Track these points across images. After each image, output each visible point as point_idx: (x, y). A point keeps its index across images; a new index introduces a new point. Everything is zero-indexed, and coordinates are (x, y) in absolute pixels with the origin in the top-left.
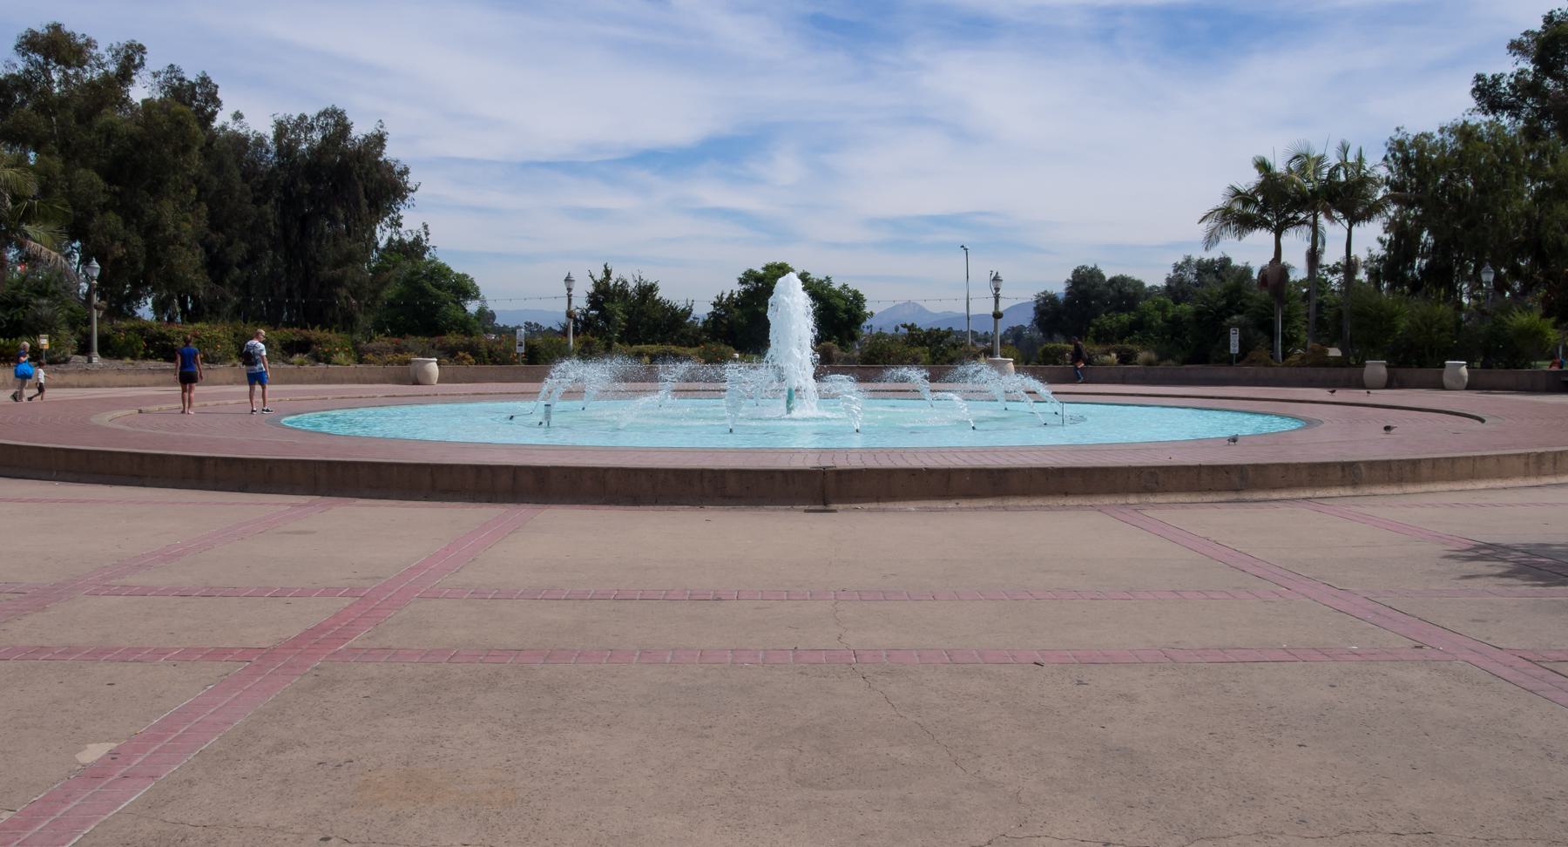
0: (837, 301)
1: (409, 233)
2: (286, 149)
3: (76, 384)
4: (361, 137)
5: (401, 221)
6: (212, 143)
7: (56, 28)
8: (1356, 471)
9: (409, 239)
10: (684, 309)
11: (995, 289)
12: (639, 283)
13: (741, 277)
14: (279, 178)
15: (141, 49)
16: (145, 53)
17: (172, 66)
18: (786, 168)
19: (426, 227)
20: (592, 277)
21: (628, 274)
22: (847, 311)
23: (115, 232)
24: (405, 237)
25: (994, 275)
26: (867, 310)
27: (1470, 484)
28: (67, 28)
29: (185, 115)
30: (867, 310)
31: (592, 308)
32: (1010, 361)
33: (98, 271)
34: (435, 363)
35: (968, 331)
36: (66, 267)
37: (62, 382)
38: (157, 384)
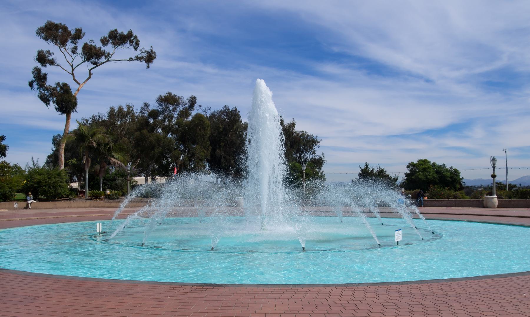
0: (446, 174)
1: (317, 156)
3: (115, 206)
4: (287, 124)
5: (316, 152)
6: (238, 129)
9: (317, 158)
10: (394, 178)
11: (493, 164)
12: (379, 170)
13: (408, 165)
15: (195, 98)
16: (196, 99)
17: (225, 106)
18: (478, 132)
19: (323, 154)
20: (360, 167)
22: (451, 177)
23: (178, 156)
25: (492, 158)
26: (461, 177)
29: (202, 118)
30: (461, 177)
32: (495, 198)
34: (496, 198)
35: (506, 185)
36: (123, 169)
37: (110, 206)
38: (90, 207)
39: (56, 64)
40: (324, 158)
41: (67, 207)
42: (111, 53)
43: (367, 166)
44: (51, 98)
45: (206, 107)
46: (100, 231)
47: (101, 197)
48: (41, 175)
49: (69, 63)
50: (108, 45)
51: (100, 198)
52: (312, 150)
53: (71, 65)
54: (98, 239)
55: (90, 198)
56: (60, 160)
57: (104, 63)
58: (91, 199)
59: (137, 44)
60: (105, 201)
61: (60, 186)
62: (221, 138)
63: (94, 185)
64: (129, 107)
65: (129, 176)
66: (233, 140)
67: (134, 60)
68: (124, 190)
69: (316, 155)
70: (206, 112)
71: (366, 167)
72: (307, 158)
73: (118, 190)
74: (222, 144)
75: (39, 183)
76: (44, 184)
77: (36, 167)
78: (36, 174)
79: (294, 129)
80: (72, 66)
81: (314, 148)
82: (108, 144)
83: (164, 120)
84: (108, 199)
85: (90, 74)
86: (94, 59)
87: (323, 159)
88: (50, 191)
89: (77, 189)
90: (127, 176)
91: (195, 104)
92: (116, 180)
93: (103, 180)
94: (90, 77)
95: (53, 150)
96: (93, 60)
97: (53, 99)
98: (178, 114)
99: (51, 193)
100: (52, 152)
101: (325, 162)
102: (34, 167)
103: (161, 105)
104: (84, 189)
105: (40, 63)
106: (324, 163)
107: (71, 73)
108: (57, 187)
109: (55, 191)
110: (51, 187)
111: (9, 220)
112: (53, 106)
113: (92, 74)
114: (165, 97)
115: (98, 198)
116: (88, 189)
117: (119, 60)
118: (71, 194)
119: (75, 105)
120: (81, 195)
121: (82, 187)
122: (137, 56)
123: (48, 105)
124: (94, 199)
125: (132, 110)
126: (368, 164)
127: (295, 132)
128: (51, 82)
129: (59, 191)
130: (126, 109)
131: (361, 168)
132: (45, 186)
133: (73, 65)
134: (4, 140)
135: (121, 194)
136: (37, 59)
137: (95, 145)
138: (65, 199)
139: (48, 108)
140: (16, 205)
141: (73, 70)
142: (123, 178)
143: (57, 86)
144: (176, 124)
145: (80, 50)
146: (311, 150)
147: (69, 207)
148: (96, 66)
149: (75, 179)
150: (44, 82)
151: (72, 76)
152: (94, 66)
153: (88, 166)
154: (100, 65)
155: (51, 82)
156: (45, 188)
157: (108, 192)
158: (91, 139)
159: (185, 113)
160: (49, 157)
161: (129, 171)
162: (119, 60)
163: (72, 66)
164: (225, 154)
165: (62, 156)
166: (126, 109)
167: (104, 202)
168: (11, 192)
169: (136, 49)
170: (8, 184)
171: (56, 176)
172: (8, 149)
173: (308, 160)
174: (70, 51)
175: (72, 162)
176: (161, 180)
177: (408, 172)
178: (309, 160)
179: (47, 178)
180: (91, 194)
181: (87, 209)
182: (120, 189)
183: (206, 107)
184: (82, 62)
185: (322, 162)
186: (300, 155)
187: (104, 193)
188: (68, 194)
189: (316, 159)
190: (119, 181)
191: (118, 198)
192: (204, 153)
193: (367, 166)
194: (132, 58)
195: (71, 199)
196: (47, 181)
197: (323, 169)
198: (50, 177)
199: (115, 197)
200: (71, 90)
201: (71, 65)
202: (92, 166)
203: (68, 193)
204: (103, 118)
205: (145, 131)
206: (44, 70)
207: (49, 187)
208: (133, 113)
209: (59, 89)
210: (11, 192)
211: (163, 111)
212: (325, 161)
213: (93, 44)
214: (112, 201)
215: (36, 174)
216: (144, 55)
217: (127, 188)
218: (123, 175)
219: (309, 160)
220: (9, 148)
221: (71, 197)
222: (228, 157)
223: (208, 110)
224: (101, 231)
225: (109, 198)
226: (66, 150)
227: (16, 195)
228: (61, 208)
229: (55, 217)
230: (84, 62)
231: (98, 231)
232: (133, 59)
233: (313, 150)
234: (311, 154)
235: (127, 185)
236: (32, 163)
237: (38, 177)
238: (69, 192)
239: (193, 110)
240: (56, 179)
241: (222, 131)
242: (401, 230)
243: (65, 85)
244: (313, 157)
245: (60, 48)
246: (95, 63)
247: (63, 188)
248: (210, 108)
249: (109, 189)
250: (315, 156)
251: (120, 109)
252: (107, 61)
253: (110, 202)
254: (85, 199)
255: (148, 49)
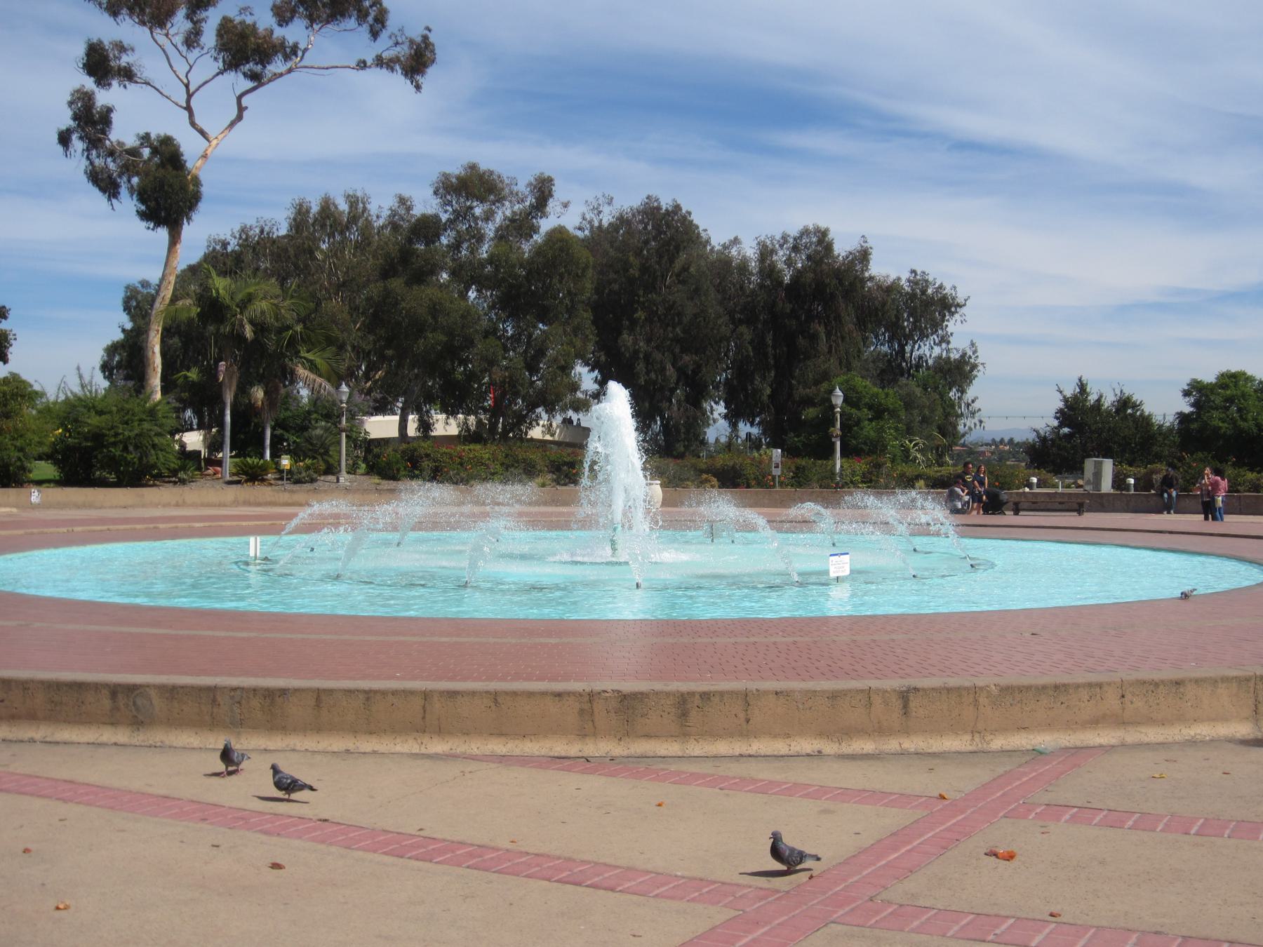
1: (955, 351)
2: (768, 271)
4: (843, 254)
6: (688, 268)
7: (473, 167)
8: (139, 702)
9: (955, 356)
13: (1186, 388)
14: (759, 299)
16: (554, 185)
19: (973, 344)
20: (1061, 392)
21: (1105, 392)
24: (952, 356)
27: (411, 742)
28: (483, 167)
31: (1061, 425)
33: (842, 399)
37: (290, 501)
38: (236, 503)
39: (139, 81)
40: (977, 357)
41: (174, 502)
42: (302, 46)
43: (1082, 387)
44: (125, 179)
45: (600, 195)
46: (256, 554)
47: (265, 477)
48: (100, 413)
49: (178, 77)
50: (294, 23)
51: (263, 480)
52: (940, 332)
53: (185, 81)
54: (251, 568)
55: (236, 478)
56: (149, 365)
57: (281, 75)
58: (238, 482)
59: (381, 20)
60: (277, 488)
61: (154, 446)
62: (636, 298)
63: (246, 441)
64: (353, 201)
65: (344, 418)
66: (675, 302)
67: (370, 67)
68: (331, 456)
69: (950, 346)
70: (600, 212)
71: (1078, 390)
72: (922, 357)
73: (314, 458)
74: (640, 315)
75: (98, 438)
76: (112, 440)
77: (88, 393)
78: (89, 411)
79: (867, 270)
80: (187, 86)
81: (947, 326)
82: (288, 328)
83: (456, 246)
84: (285, 482)
85: (241, 109)
86: (251, 64)
87: (972, 361)
88: (126, 458)
89: (200, 452)
90: (340, 416)
91: (551, 200)
92: (309, 428)
93: (273, 429)
94: (240, 117)
95: (124, 331)
96: (248, 66)
97: (129, 181)
98: (497, 230)
99: (128, 463)
100: (119, 336)
101: (978, 371)
102: (84, 391)
103: (450, 203)
104: (219, 453)
105: (92, 79)
106: (975, 373)
107: (185, 105)
108: (145, 448)
109: (140, 459)
110: (131, 448)
111: (42, 533)
112: (128, 204)
113: (246, 108)
114: (458, 178)
115: (258, 480)
116: (231, 452)
117: (326, 66)
118: (183, 468)
119: (193, 200)
120: (211, 471)
121: (214, 445)
122: (381, 56)
123: (114, 201)
124: (246, 481)
125: (365, 209)
126: (1085, 382)
127: (871, 278)
128: (123, 132)
129: (152, 459)
130: (343, 206)
131: (1065, 393)
132: (114, 444)
133: (189, 82)
134: (5, 318)
135: (323, 467)
136: (84, 65)
137: (249, 332)
138: (167, 479)
139: (113, 208)
140: (35, 495)
141: (190, 96)
142: (328, 422)
143: (142, 144)
144: (491, 260)
145: (209, 38)
146: (937, 331)
147: (177, 502)
148: (256, 84)
149: (190, 417)
150: (104, 132)
151: (186, 114)
152: (250, 84)
153: (230, 390)
154: (270, 81)
155: (123, 132)
156: (113, 450)
157: (286, 462)
158: (241, 313)
159: (521, 226)
160: (112, 349)
161: (344, 405)
162: (327, 68)
163: (187, 86)
164: (648, 346)
165: (153, 352)
166: (343, 206)
167: (273, 491)
168: (23, 459)
169: (375, 35)
170: (14, 439)
171: (144, 417)
172: (12, 342)
173: (927, 361)
174: (178, 40)
175: (186, 377)
176: (447, 427)
177: (1187, 409)
178: (930, 362)
179: (121, 423)
180: (239, 467)
181: (228, 508)
182: (320, 454)
183: (600, 195)
184: (218, 74)
185: (971, 370)
186: (902, 347)
187: (274, 466)
188: (177, 467)
189: (952, 359)
190: (319, 429)
191: (312, 481)
192: (574, 347)
193: (1082, 387)
194: (364, 62)
195: (183, 482)
196: (120, 431)
197: (971, 393)
198: (128, 420)
199: (304, 478)
200: (182, 155)
201: (185, 81)
202: (243, 390)
203: (175, 463)
204: (273, 234)
205: (397, 284)
206: (103, 98)
207: (125, 449)
208: (367, 219)
209: (146, 152)
210: (23, 459)
211: (456, 219)
212: (980, 368)
213: (249, 20)
214: (297, 487)
215: (89, 411)
216: (404, 51)
217: (340, 452)
218: (329, 413)
219: (930, 362)
220: (15, 339)
221: (185, 477)
222: (657, 356)
223: (606, 206)
224: (258, 554)
225: (287, 479)
226: (167, 333)
227: (35, 470)
228: (156, 505)
229: (152, 526)
230: (221, 73)
231: (252, 554)
232: (368, 64)
233: (942, 329)
234: (934, 343)
235: (339, 443)
236: (78, 381)
237: (94, 420)
238: (179, 462)
239: (544, 215)
240: (143, 426)
241: (637, 275)
242: (847, 554)
243: (167, 141)
244: (944, 355)
245: (152, 33)
246: (255, 77)
247: (161, 450)
248: (612, 199)
249: (287, 454)
250: (948, 351)
251: (327, 207)
252: (290, 71)
253: (292, 492)
254: (221, 480)
255: (416, 34)
